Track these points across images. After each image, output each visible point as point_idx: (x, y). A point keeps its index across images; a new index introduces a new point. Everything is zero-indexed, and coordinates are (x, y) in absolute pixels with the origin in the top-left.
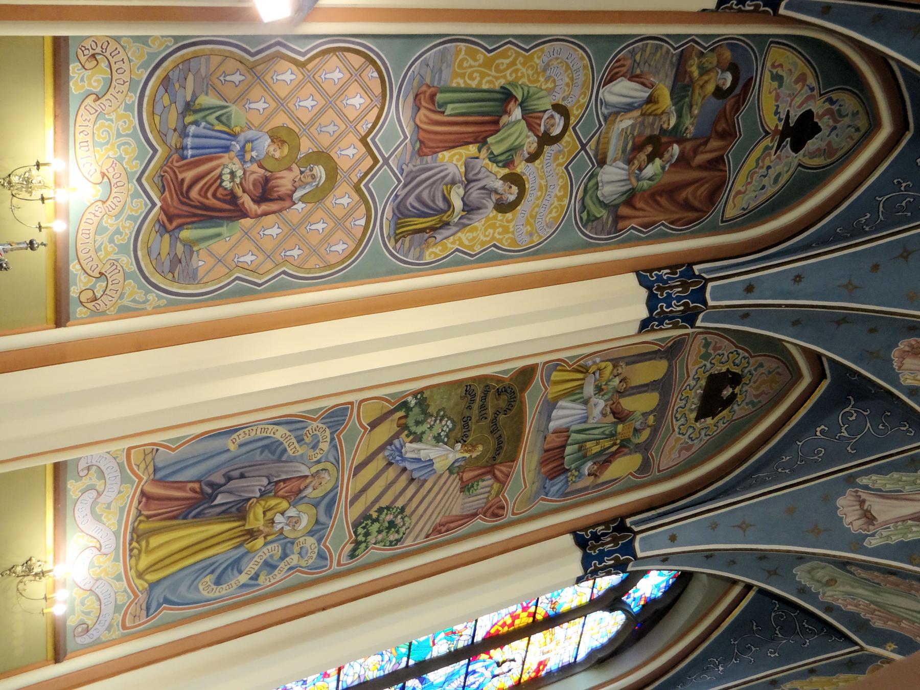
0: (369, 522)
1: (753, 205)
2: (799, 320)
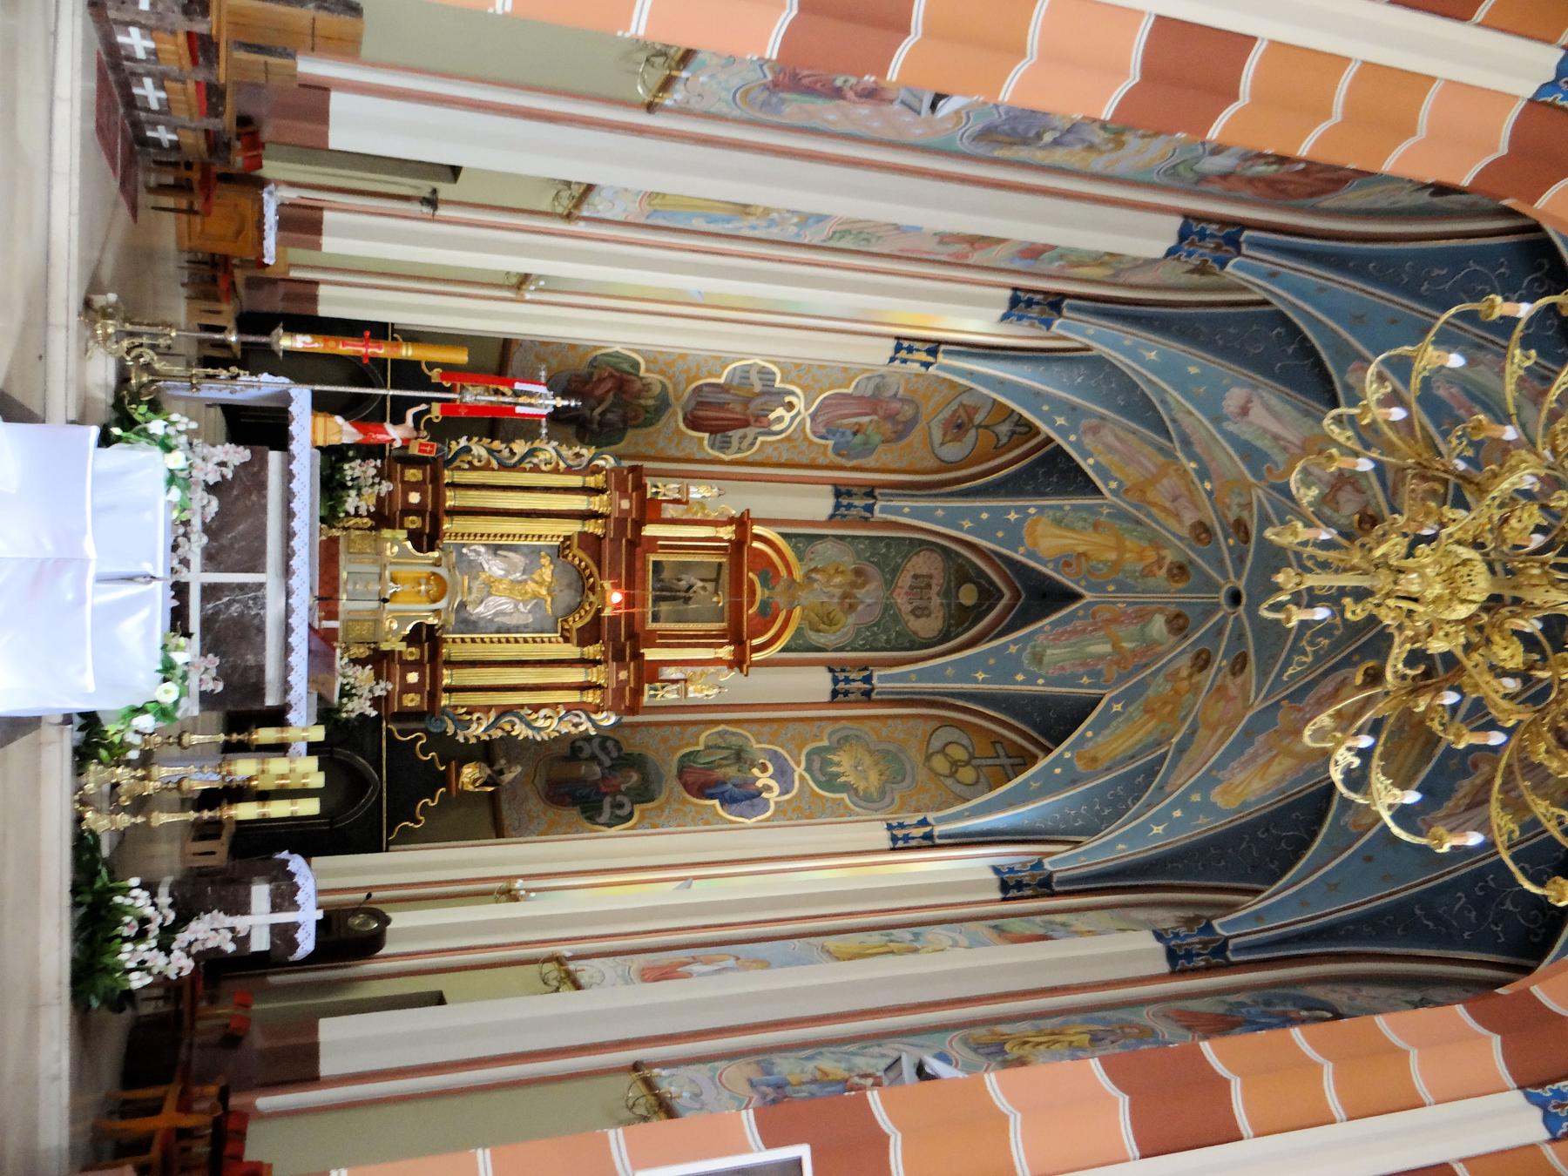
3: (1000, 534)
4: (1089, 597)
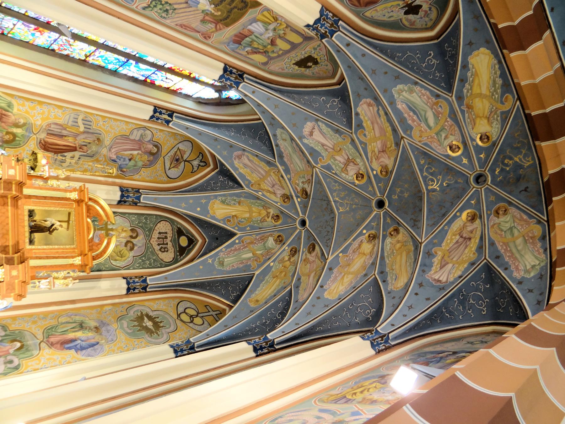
0: (159, 3)
1: (375, 18)
2: (351, 67)
3: (199, 209)
4: (239, 234)
